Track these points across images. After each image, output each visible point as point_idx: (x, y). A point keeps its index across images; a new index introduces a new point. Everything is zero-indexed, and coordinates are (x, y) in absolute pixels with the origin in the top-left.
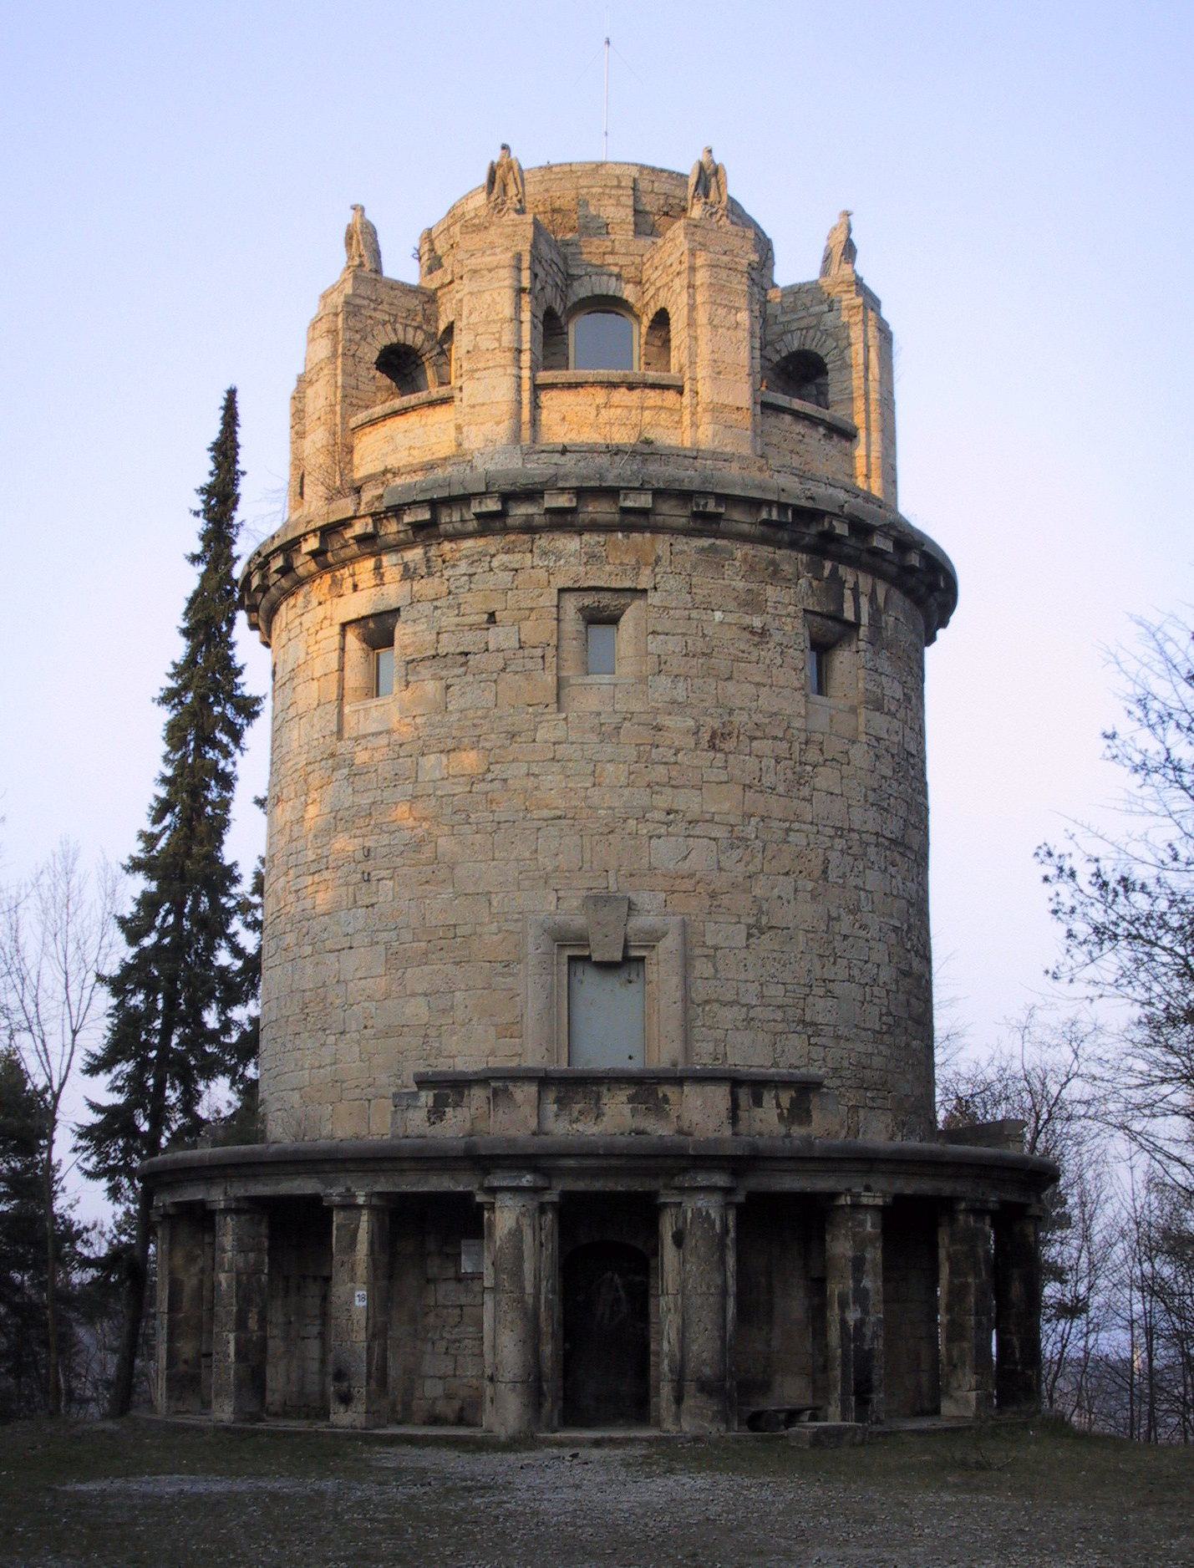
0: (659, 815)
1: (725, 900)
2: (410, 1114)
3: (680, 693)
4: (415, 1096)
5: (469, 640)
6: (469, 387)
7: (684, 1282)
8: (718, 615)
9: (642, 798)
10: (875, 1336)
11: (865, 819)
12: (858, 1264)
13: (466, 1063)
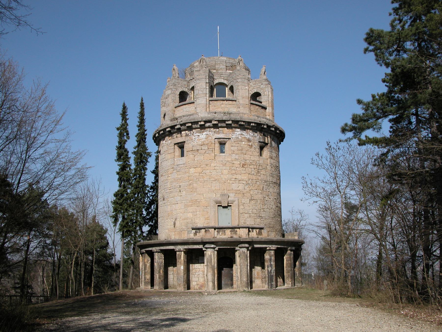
0: (234, 179)
1: (245, 195)
2: (191, 234)
3: (237, 157)
4: (192, 231)
5: (199, 148)
6: (198, 101)
7: (240, 264)
8: (243, 143)
9: (231, 176)
10: (273, 273)
11: (269, 179)
12: (270, 260)
13: (200, 225)
